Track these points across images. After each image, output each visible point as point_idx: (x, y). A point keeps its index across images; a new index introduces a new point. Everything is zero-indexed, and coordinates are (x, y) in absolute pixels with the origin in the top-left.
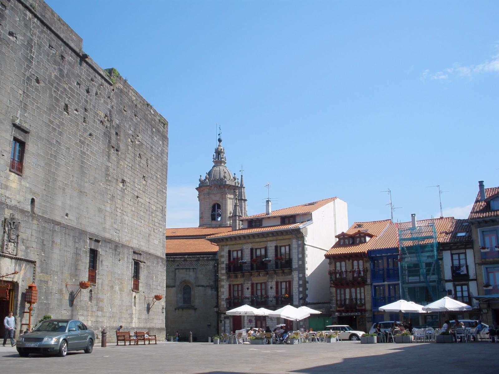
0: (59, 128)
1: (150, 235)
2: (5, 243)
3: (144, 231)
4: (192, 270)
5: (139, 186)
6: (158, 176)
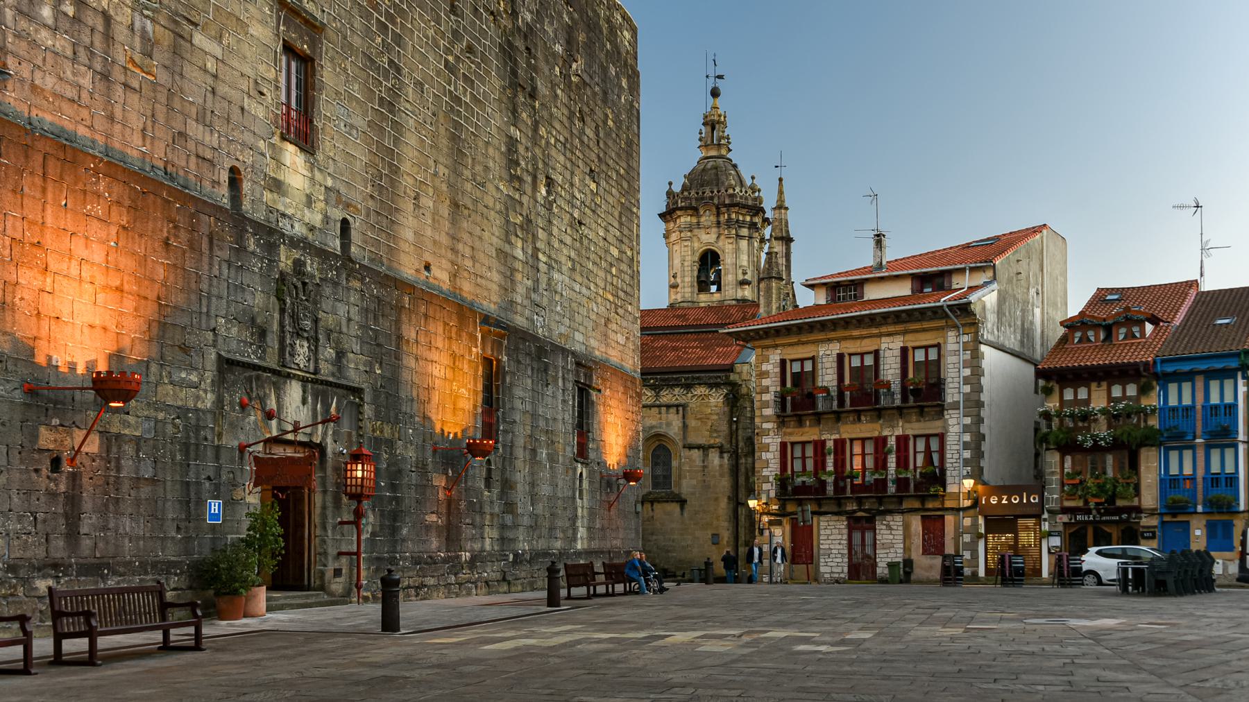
0: (394, 23)
1: (608, 320)
2: (288, 341)
3: (595, 310)
5: (583, 196)
6: (622, 171)
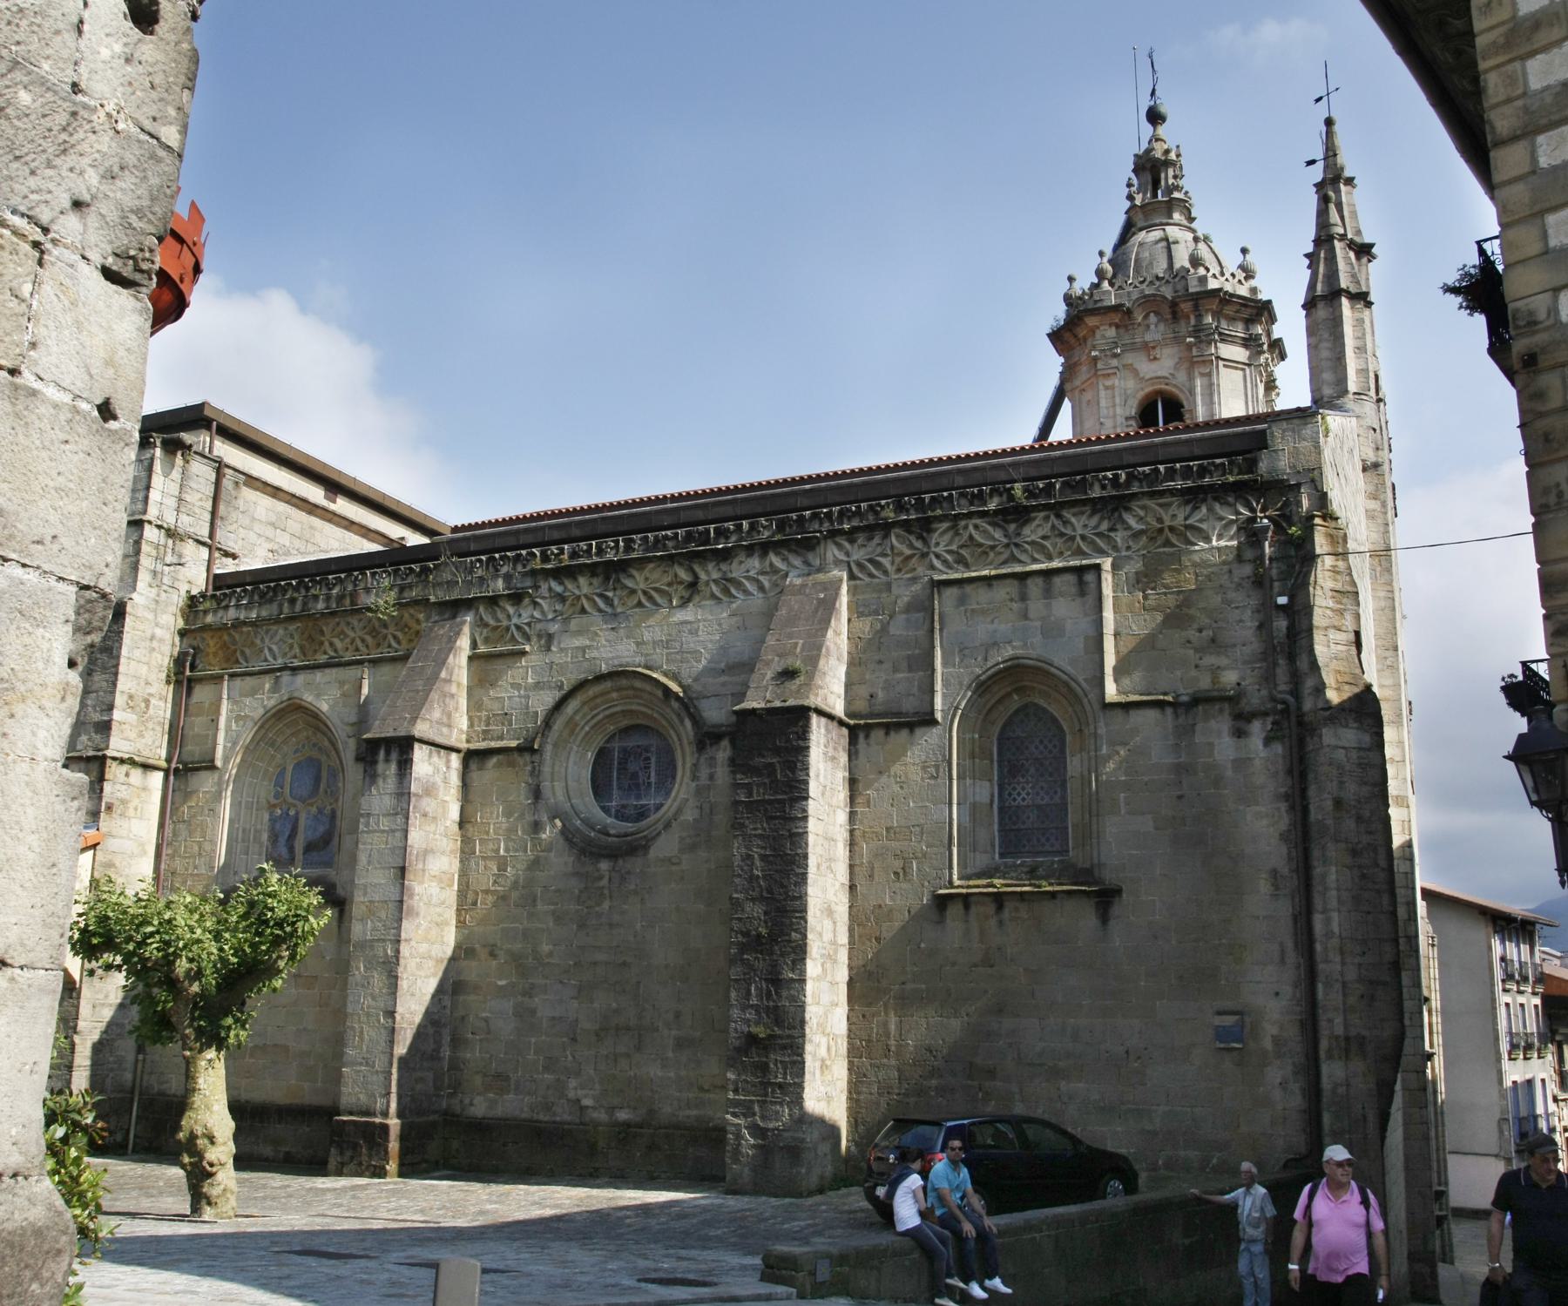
4: (1063, 583)
